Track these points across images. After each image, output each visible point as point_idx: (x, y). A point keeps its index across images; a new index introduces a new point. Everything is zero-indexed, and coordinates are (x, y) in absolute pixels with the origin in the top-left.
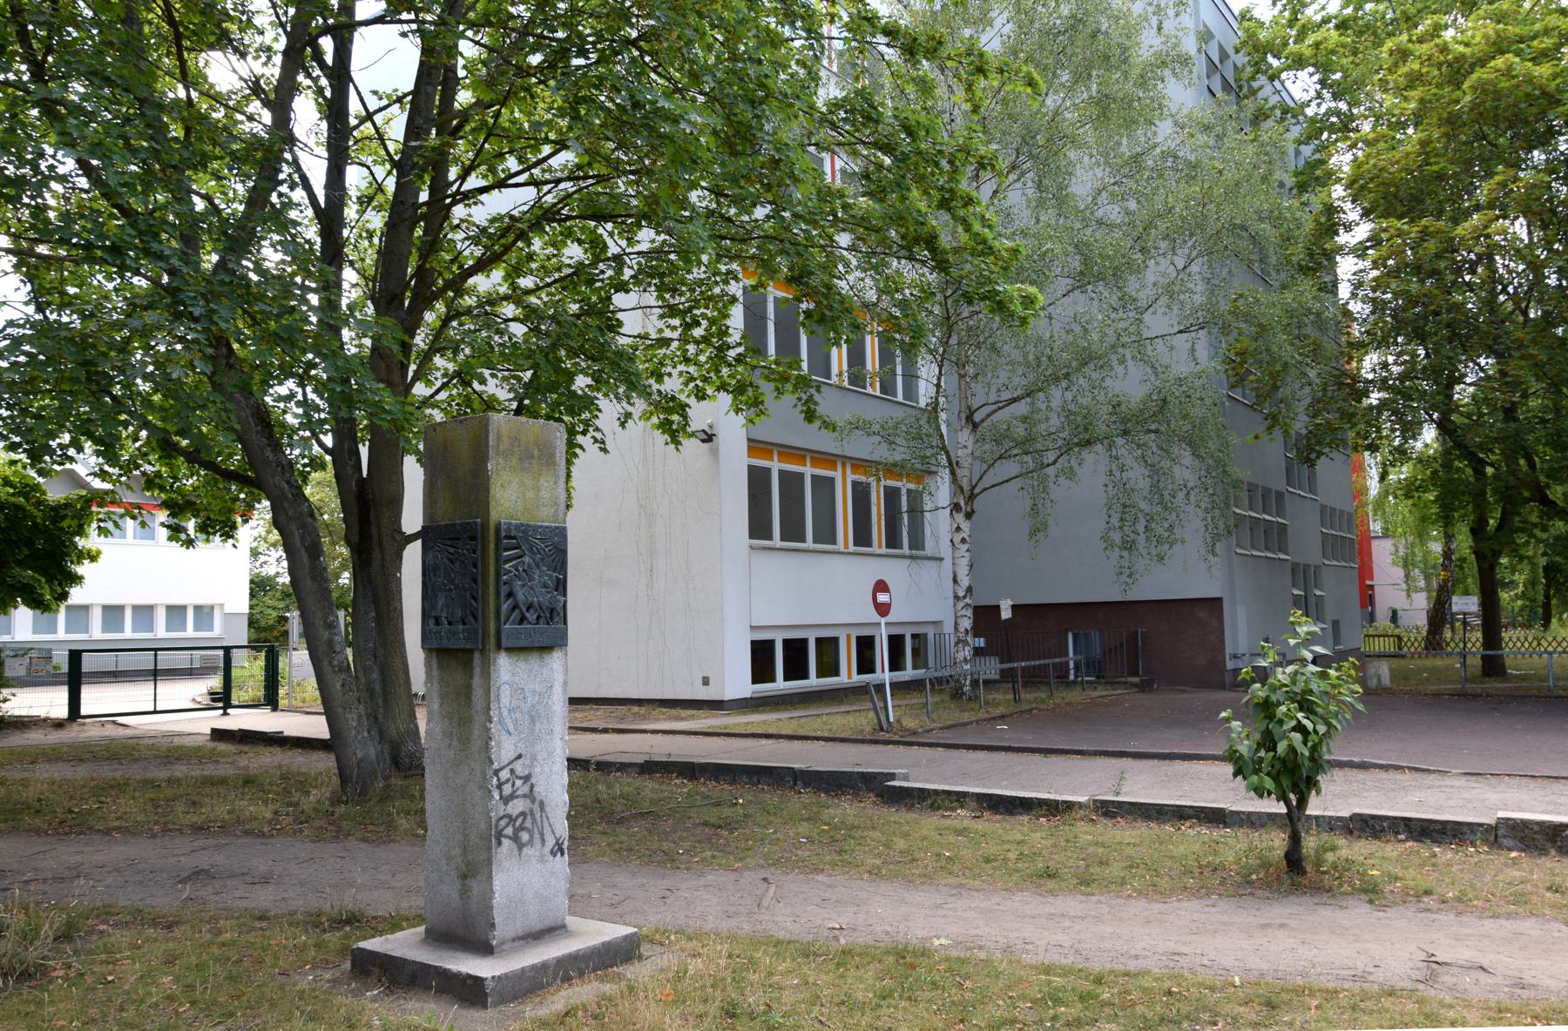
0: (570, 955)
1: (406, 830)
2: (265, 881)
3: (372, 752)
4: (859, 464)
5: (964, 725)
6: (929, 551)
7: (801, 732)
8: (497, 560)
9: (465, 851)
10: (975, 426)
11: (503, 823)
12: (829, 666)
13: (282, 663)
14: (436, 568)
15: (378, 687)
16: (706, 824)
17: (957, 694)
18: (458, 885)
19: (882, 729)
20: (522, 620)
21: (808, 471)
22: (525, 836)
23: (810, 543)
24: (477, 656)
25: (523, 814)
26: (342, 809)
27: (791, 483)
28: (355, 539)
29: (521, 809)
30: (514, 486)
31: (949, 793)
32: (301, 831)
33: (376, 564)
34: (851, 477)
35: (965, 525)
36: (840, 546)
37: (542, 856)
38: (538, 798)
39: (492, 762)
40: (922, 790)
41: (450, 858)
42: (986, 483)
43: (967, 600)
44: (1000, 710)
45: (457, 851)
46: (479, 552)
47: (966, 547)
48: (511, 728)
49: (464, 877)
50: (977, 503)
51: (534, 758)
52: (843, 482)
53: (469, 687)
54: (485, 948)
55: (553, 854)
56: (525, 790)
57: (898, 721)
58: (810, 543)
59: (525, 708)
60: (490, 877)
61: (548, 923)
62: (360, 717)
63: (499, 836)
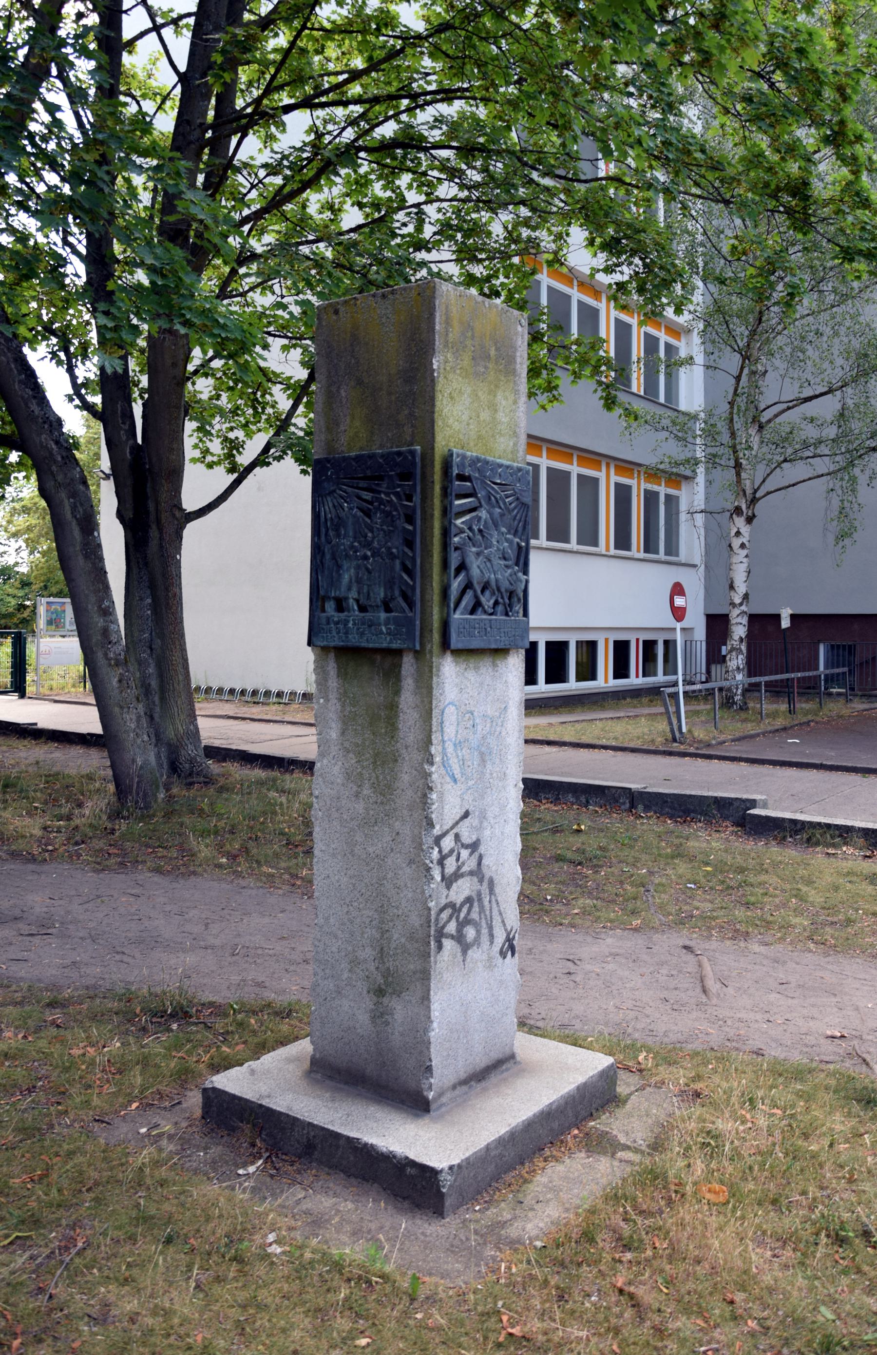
0: (542, 1112)
1: (207, 859)
2: (44, 928)
3: (152, 759)
4: (625, 466)
5: (752, 737)
6: (683, 557)
7: (585, 740)
8: (445, 511)
9: (382, 955)
10: (761, 427)
11: (445, 915)
12: (588, 672)
13: (31, 650)
14: (339, 524)
15: (154, 683)
16: (559, 859)
17: (728, 703)
18: (368, 1002)
19: (674, 740)
20: (476, 606)
21: (575, 469)
22: (470, 933)
23: (573, 545)
24: (408, 663)
25: (469, 900)
26: (122, 826)
27: (559, 479)
28: (130, 514)
29: (466, 893)
30: (466, 399)
31: (828, 826)
32: (79, 856)
33: (153, 546)
34: (614, 478)
35: (745, 530)
36: (602, 548)
37: (490, 959)
38: (487, 873)
39: (431, 825)
40: (794, 822)
41: (355, 962)
42: (769, 486)
43: (744, 608)
44: (779, 723)
45: (368, 953)
46: (417, 498)
47: (744, 552)
48: (458, 776)
49: (380, 992)
50: (759, 507)
51: (483, 817)
52: (607, 481)
53: (392, 708)
54: (416, 1103)
55: (503, 954)
56: (471, 865)
57: (690, 731)
58: (573, 545)
59: (474, 740)
60: (426, 999)
61: (495, 1055)
62: (139, 718)
63: (441, 934)
